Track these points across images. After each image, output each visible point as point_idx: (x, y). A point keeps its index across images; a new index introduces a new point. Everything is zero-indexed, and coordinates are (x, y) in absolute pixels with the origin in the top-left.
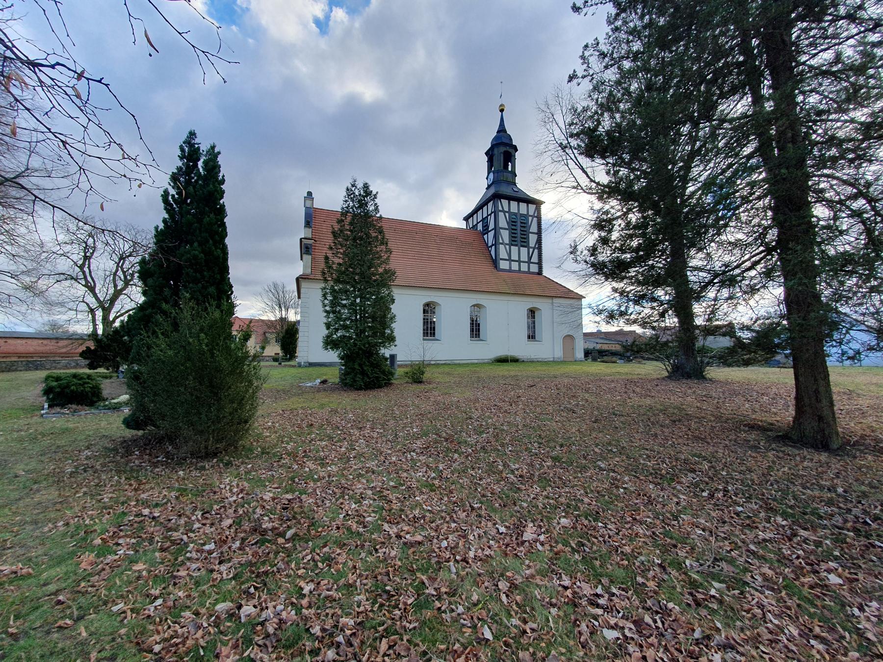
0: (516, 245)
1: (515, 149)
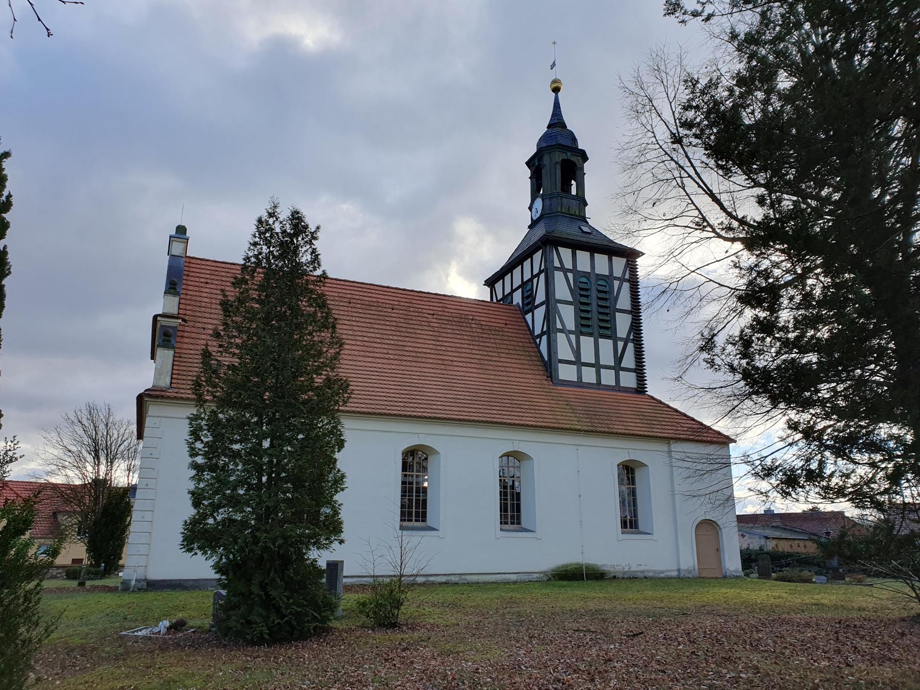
0: (590, 335)
1: (584, 156)
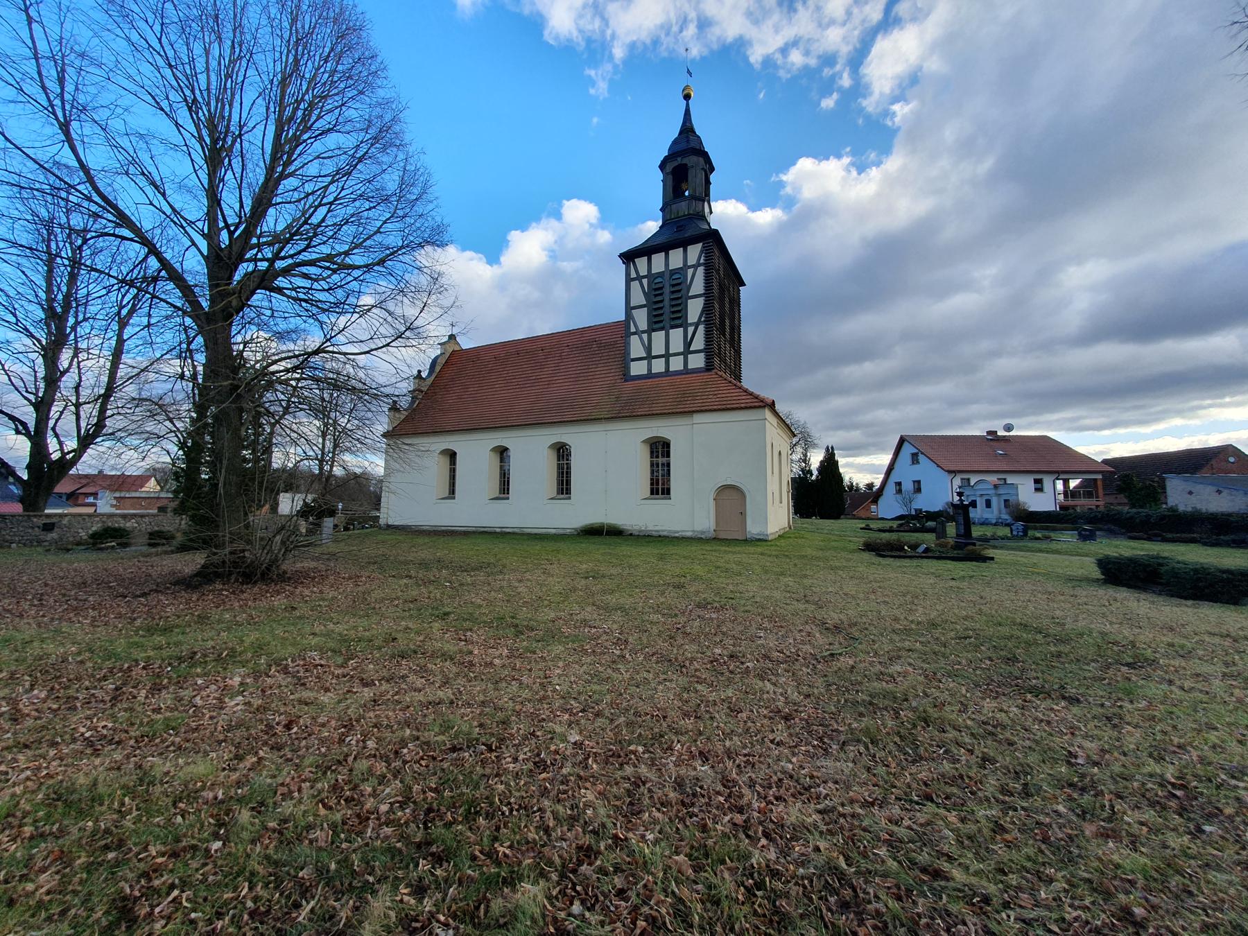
0: (662, 329)
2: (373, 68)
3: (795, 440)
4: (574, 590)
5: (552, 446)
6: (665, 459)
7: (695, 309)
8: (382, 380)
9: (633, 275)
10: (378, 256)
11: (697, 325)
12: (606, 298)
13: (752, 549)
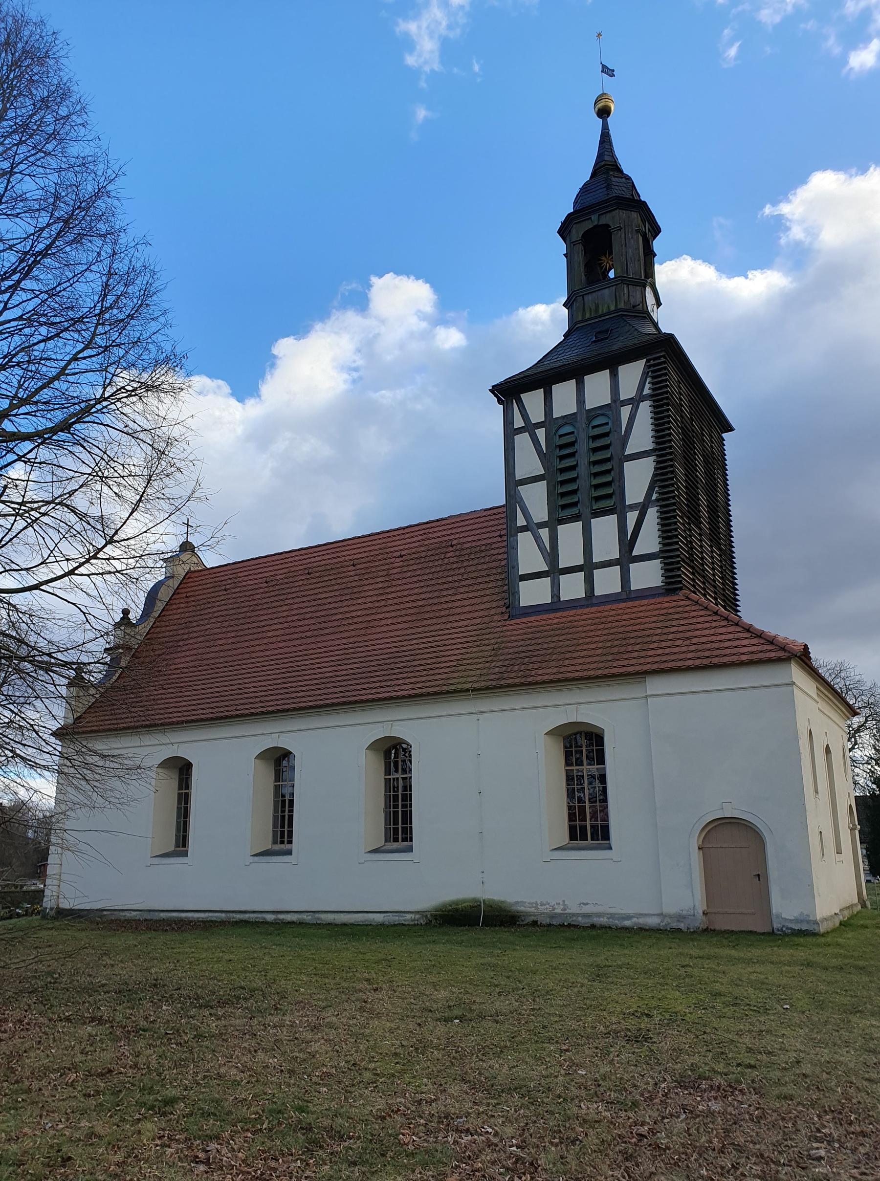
2: (63, 111)
3: (857, 721)
4: (422, 1047)
5: (375, 746)
6: (594, 768)
7: (637, 479)
8: (60, 636)
9: (519, 422)
10: (59, 416)
11: (643, 509)
12: (466, 461)
13: (785, 953)
